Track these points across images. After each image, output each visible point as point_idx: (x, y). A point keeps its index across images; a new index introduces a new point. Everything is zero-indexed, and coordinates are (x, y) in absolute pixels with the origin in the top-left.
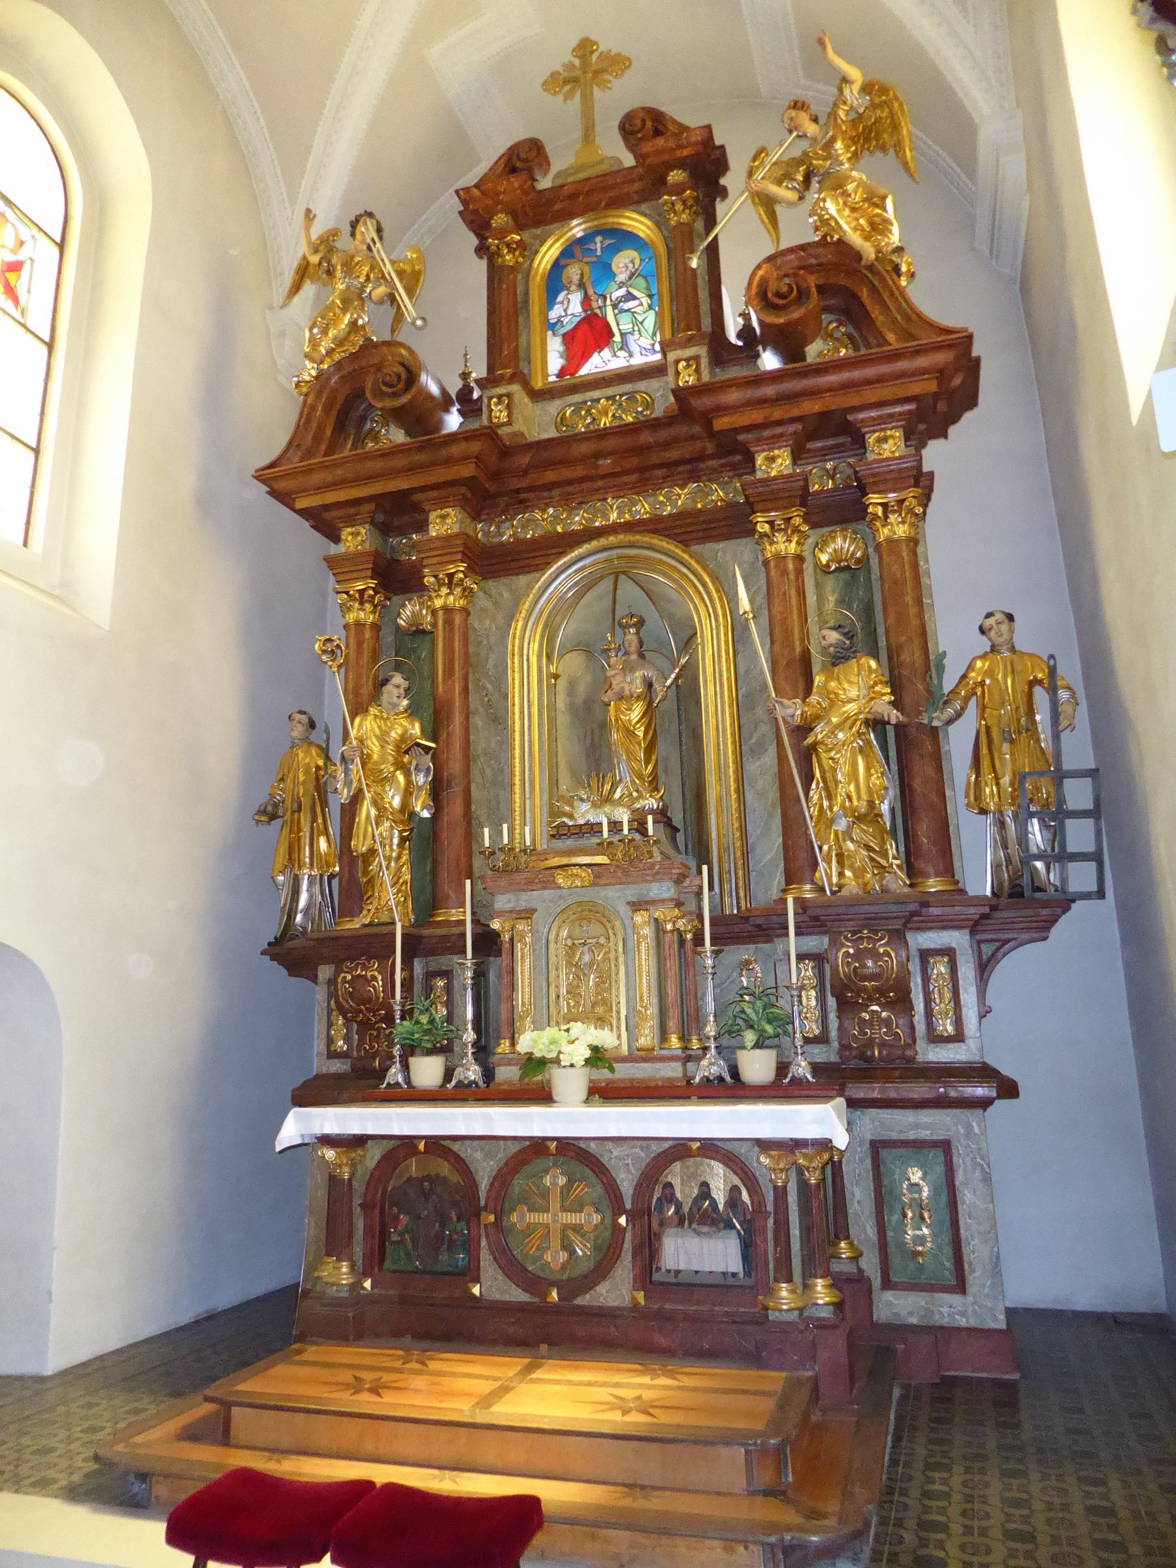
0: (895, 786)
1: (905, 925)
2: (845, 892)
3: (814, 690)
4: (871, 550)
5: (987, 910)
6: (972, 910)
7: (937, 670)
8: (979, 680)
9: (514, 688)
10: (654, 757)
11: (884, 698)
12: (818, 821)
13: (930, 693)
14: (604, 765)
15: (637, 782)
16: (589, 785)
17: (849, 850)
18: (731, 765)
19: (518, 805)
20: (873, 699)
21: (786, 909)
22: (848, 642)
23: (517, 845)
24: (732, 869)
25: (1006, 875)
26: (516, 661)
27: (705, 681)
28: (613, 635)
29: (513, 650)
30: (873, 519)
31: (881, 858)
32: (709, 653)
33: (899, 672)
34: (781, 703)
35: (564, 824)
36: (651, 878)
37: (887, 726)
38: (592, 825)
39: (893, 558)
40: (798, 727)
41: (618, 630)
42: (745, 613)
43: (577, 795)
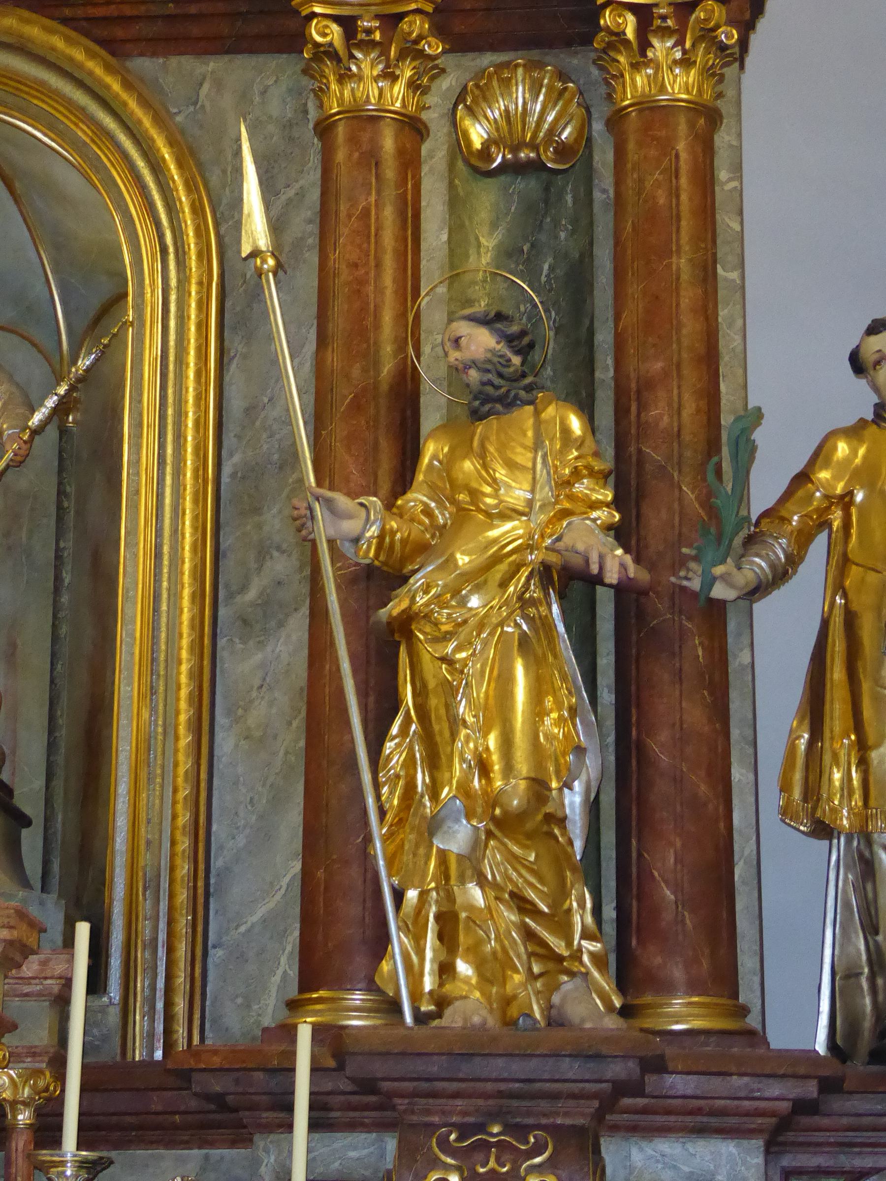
0: (603, 748)
1: (599, 1116)
2: (452, 1018)
3: (420, 477)
4: (598, 126)
5: (811, 1089)
6: (775, 1089)
7: (735, 456)
8: (839, 489)
11: (595, 514)
12: (400, 822)
13: (713, 513)
17: (471, 907)
18: (184, 654)
20: (565, 513)
21: (293, 1054)
22: (516, 360)
24: (162, 937)
25: (868, 1001)
27: (137, 425)
30: (610, 46)
31: (552, 932)
33: (640, 451)
34: (329, 504)
37: (599, 588)
39: (653, 153)
40: (370, 571)
42: (255, 253)
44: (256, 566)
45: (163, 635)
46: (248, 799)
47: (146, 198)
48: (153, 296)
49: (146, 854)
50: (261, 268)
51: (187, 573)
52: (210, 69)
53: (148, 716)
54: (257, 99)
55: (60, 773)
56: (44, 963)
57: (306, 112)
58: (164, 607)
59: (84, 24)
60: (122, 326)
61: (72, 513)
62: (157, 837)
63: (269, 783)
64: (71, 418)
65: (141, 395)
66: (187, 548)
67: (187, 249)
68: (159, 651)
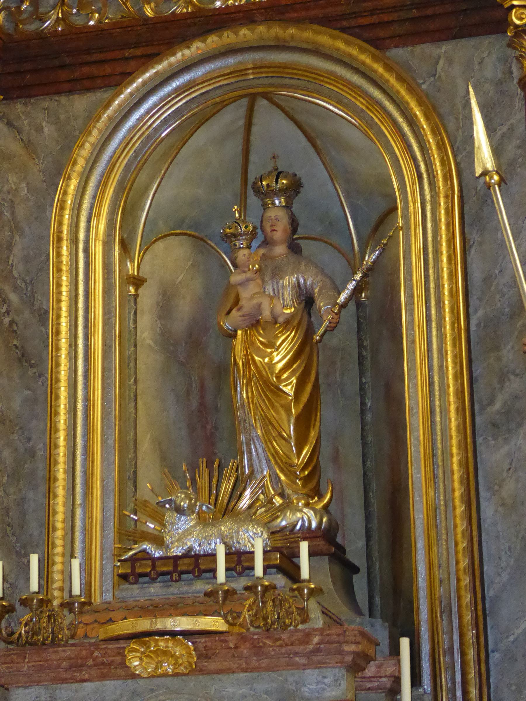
9: (59, 301)
10: (313, 434)
14: (221, 447)
15: (283, 477)
16: (194, 481)
18: (455, 450)
19: (60, 517)
23: (56, 593)
24: (456, 646)
26: (65, 251)
27: (410, 296)
28: (244, 209)
29: (60, 232)
32: (416, 245)
35: (145, 555)
36: (304, 661)
38: (197, 557)
41: (253, 200)
42: (485, 173)
43: (170, 502)
44: (499, 386)
45: (439, 438)
46: (507, 548)
47: (406, 143)
48: (415, 208)
49: (440, 589)
50: (490, 183)
51: (452, 394)
52: (443, 51)
53: (433, 494)
54: (477, 67)
55: (375, 537)
56: (379, 667)
57: (511, 73)
58: (438, 419)
59: (357, 30)
60: (395, 230)
61: (369, 359)
62: (446, 576)
63: (520, 537)
64: (363, 295)
65: (411, 275)
66: (451, 377)
67: (435, 174)
68: (437, 449)
